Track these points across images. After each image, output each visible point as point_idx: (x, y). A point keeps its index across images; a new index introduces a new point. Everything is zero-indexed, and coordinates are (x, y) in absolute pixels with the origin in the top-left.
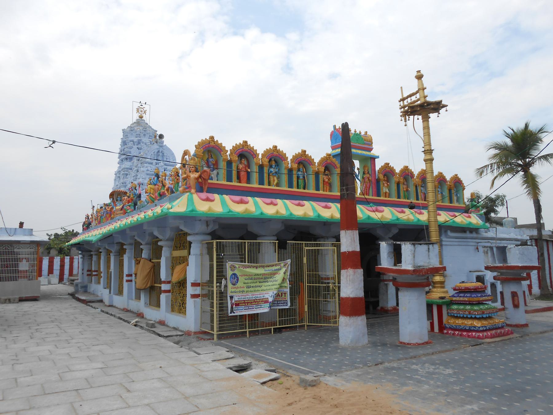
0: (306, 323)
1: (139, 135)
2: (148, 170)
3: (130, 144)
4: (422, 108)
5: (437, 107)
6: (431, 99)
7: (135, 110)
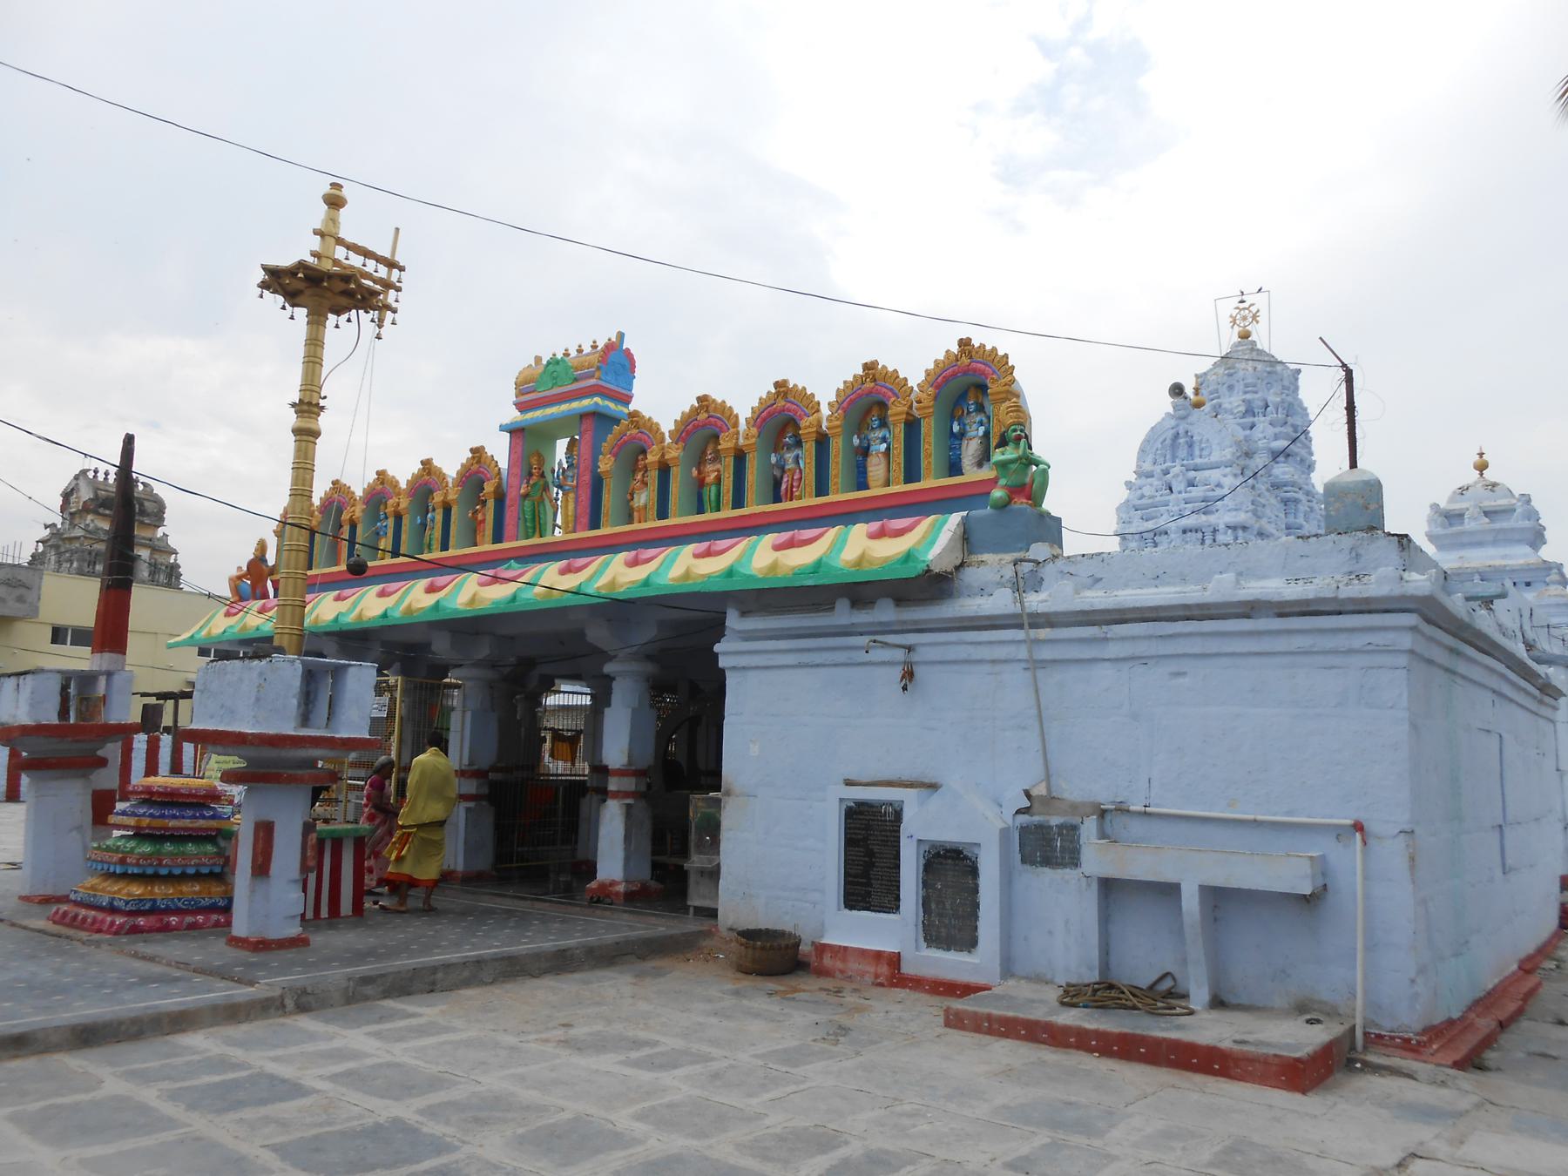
1: (1216, 391)
2: (1142, 497)
7: (1226, 322)
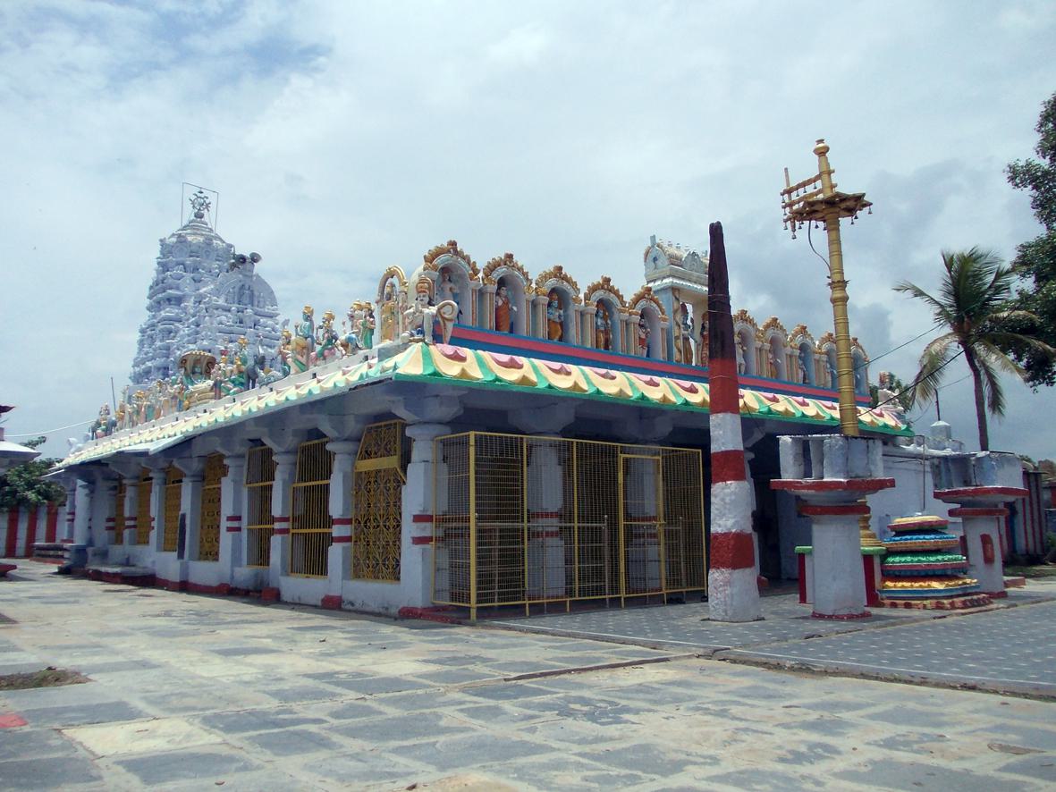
0: (623, 595)
3: (178, 271)
4: (829, 208)
5: (853, 204)
6: (846, 187)
